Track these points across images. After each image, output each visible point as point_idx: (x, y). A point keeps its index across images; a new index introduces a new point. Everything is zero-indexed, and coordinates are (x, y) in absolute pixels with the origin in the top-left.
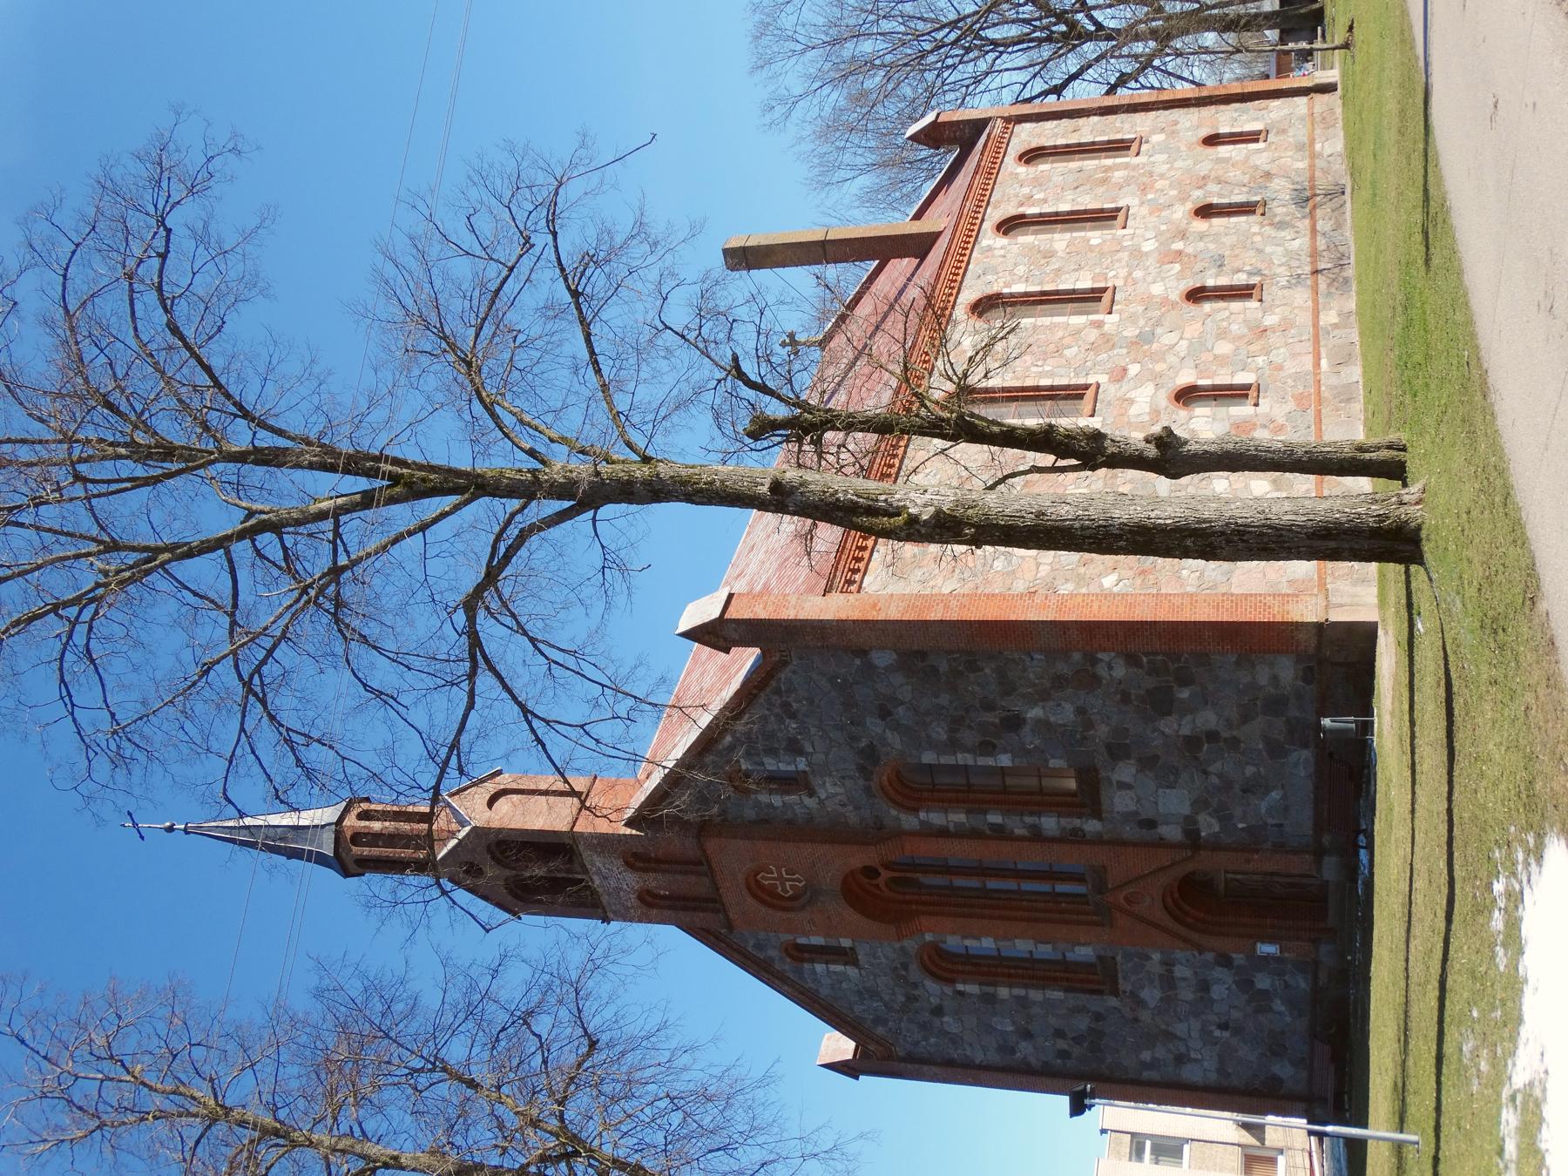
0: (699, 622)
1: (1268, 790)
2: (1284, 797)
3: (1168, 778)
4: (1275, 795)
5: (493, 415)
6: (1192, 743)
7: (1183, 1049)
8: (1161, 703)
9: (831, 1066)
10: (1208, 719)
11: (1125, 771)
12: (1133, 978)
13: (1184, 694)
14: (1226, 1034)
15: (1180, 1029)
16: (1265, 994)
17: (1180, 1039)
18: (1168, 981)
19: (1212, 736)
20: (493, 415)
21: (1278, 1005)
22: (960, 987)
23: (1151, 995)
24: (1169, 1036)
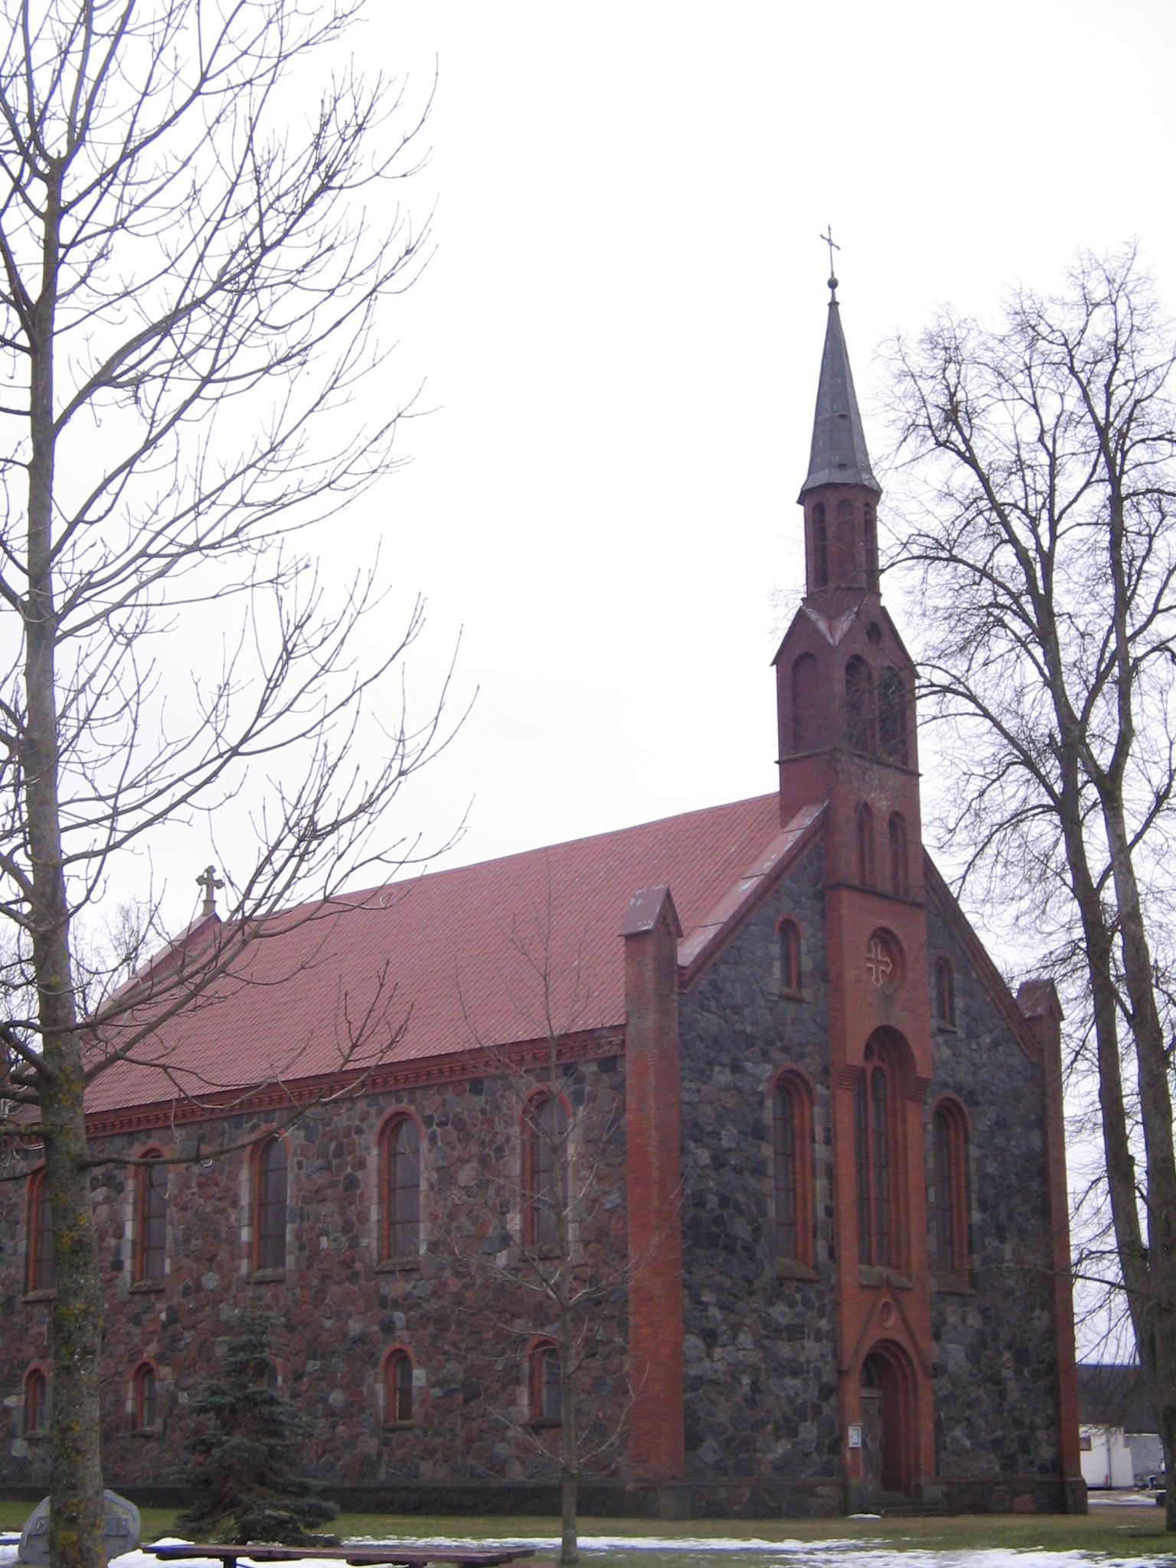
0: (861, 412)
1: (970, 1437)
2: (967, 1451)
3: (974, 1357)
4: (968, 1443)
5: (228, 1151)
6: (996, 1380)
7: (724, 1339)
8: (1021, 1357)
9: (668, 896)
10: (1014, 1395)
11: (974, 1321)
12: (798, 1297)
13: (1026, 1372)
14: (746, 1389)
15: (745, 1339)
16: (793, 1433)
17: (735, 1338)
18: (794, 1333)
19: (1002, 1395)
20: (228, 1151)
21: (781, 1448)
22: (769, 1103)
23: (780, 1312)
24: (736, 1328)
